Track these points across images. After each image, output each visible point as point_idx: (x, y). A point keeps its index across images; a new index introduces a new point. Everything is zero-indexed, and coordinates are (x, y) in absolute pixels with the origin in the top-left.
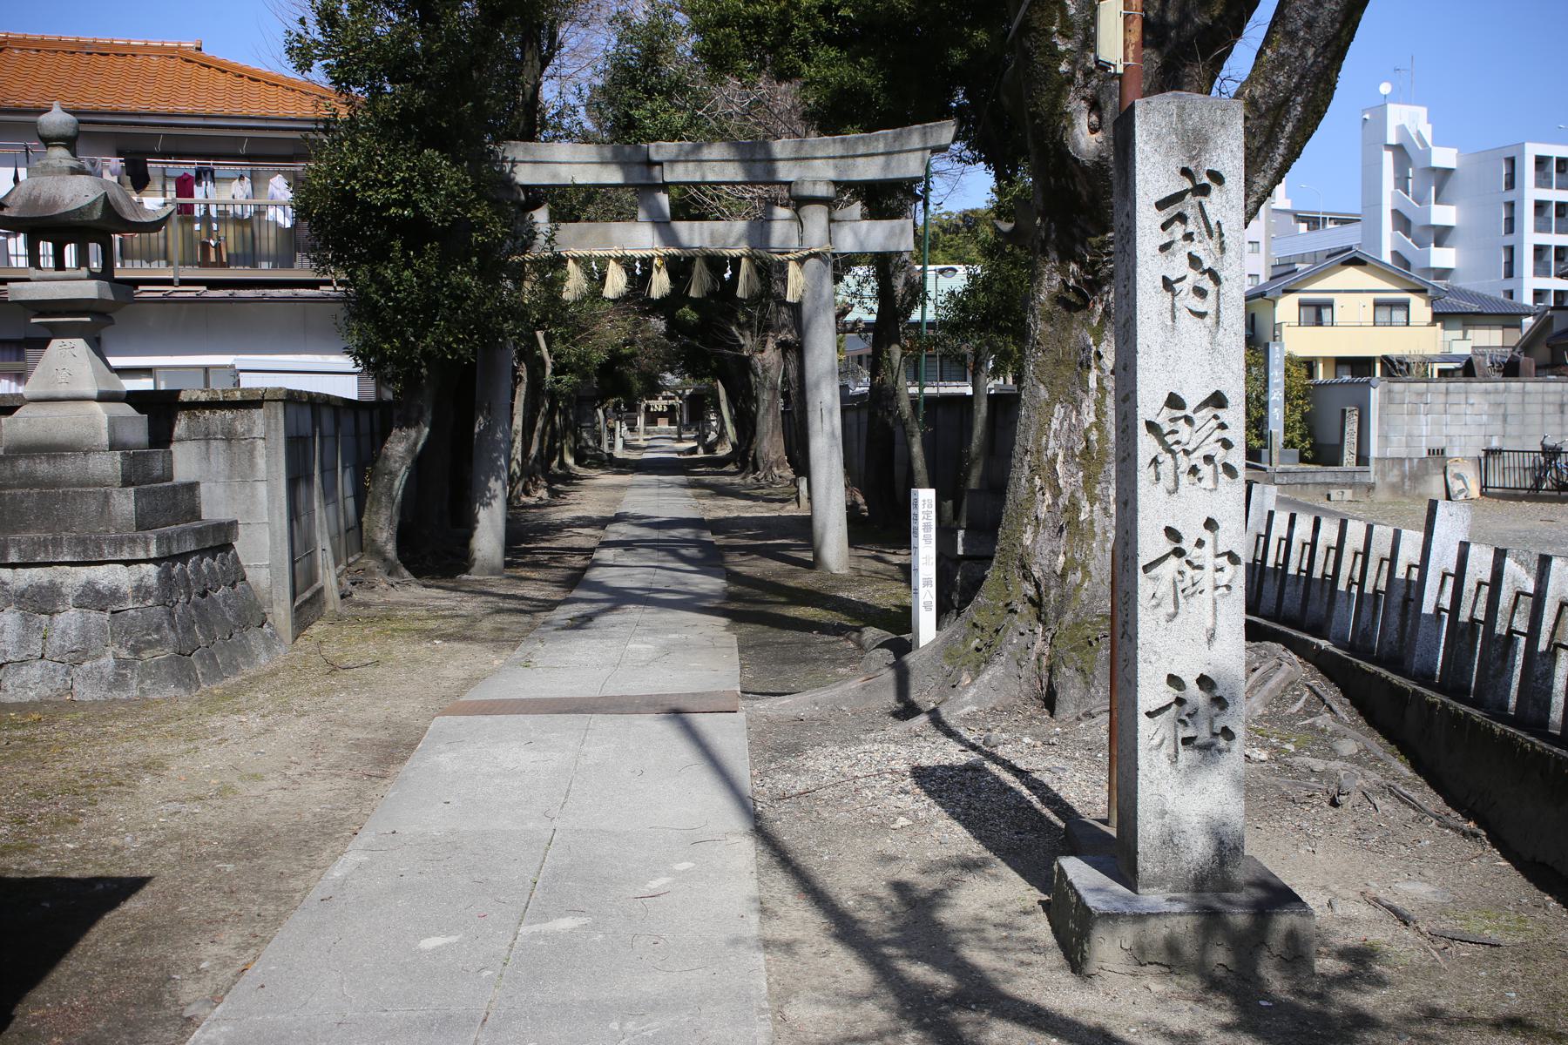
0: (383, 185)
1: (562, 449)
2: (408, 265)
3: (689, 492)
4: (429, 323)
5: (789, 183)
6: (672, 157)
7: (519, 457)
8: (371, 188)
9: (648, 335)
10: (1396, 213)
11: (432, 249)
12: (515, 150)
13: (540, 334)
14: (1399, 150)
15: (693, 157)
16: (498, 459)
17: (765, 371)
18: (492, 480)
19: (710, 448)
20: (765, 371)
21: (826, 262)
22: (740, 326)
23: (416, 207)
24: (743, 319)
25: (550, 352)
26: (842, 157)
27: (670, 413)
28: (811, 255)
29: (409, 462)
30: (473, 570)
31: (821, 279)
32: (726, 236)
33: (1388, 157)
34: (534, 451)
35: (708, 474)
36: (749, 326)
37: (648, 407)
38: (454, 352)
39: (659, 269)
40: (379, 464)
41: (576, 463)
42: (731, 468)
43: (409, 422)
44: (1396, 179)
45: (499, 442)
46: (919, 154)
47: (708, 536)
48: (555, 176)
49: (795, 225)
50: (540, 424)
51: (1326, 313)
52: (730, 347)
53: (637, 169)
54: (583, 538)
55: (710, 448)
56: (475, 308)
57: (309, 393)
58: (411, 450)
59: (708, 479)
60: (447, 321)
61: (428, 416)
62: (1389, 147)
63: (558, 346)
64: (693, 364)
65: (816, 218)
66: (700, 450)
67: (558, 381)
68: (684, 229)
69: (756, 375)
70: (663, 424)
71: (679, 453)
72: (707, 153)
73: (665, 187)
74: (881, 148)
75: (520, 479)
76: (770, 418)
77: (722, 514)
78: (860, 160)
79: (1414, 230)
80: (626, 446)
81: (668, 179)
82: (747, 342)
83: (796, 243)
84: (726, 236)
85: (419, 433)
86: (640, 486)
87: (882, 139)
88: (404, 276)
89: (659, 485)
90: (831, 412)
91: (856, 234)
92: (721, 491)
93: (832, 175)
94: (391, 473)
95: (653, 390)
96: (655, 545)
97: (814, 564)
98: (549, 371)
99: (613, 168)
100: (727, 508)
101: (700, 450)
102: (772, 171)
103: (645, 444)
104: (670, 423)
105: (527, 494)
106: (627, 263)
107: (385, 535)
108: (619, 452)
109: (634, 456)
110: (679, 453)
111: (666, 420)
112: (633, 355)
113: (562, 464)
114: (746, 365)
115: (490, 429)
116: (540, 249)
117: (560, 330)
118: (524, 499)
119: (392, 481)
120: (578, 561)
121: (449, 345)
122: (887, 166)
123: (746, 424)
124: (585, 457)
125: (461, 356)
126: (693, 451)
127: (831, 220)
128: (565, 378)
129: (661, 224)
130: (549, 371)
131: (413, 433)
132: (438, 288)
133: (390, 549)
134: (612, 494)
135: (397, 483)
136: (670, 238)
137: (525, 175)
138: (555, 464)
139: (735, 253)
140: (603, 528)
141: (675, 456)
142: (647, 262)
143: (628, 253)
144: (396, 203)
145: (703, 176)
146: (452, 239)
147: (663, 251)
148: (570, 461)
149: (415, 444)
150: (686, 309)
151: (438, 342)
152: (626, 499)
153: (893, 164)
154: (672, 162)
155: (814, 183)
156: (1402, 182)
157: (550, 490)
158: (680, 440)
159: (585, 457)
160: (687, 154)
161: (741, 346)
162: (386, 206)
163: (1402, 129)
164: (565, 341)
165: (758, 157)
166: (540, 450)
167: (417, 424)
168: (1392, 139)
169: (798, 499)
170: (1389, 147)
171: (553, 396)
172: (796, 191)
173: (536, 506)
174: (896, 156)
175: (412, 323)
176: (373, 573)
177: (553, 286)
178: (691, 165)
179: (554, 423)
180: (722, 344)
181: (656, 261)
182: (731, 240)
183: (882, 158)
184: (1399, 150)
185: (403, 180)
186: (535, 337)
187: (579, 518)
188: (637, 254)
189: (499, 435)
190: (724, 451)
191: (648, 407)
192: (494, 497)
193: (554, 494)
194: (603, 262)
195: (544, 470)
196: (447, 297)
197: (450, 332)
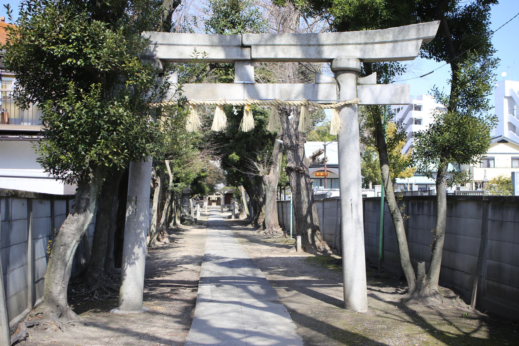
0: (63, 42)
1: (175, 217)
2: (79, 98)
3: (236, 239)
4: (94, 141)
5: (330, 61)
6: (256, 42)
7: (155, 223)
8: (54, 44)
9: (211, 168)
10: (510, 124)
11: (96, 87)
12: (157, 37)
13: (167, 162)
14: (510, 98)
15: (270, 43)
16: (140, 233)
17: (270, 183)
18: (136, 247)
19: (237, 216)
20: (270, 183)
21: (354, 109)
22: (258, 162)
23: (86, 59)
24: (259, 159)
25: (172, 171)
26: (366, 44)
27: (218, 202)
28: (346, 105)
29: (78, 237)
30: (121, 307)
31: (351, 120)
32: (289, 93)
33: (506, 101)
34: (162, 220)
35: (240, 229)
36: (262, 162)
37: (209, 198)
38: (110, 161)
39: (247, 112)
40: (57, 238)
41: (181, 223)
42: (250, 226)
43: (79, 209)
44: (509, 110)
45: (141, 223)
46: (414, 42)
47: (261, 274)
48: (181, 54)
49: (335, 86)
50: (166, 207)
51: (491, 162)
52: (254, 172)
53: (235, 50)
54: (186, 273)
55: (237, 216)
56: (127, 130)
57: (9, 190)
58: (79, 229)
59: (242, 232)
60: (106, 139)
61: (93, 206)
62: (506, 97)
63: (176, 169)
64: (231, 180)
65: (348, 81)
66: (233, 217)
67: (176, 186)
68: (262, 88)
69: (265, 185)
70: (214, 205)
71: (224, 218)
72: (278, 40)
73: (252, 61)
74: (391, 38)
75: (155, 234)
76: (272, 204)
77: (258, 255)
78: (377, 46)
79: (517, 130)
80: (202, 215)
81: (254, 56)
82: (261, 170)
83: (334, 97)
84: (289, 93)
85: (86, 217)
86: (212, 236)
87: (391, 33)
88: (76, 108)
89: (221, 235)
90: (357, 206)
91: (373, 93)
92: (252, 240)
93: (359, 55)
94: (65, 245)
95: (213, 191)
96: (233, 281)
97: (343, 305)
98: (171, 181)
99: (219, 49)
100: (258, 250)
101: (233, 217)
102: (319, 52)
103: (208, 213)
104: (217, 204)
105: (158, 240)
106: (227, 109)
107: (59, 288)
108: (199, 218)
109: (204, 219)
110: (224, 218)
111: (215, 203)
112: (206, 176)
113: (175, 224)
114: (259, 180)
115: (135, 214)
116: (172, 97)
117: (178, 161)
118: (157, 243)
119: (65, 250)
120: (187, 294)
121: (106, 157)
122: (394, 49)
123: (256, 207)
124: (184, 220)
125: (115, 165)
126: (230, 217)
127: (358, 84)
128: (179, 185)
129: (248, 85)
130: (171, 181)
131: (81, 217)
132: (100, 116)
133: (62, 299)
134: (199, 240)
135: (69, 252)
136: (254, 94)
137: (162, 53)
138: (171, 224)
139: (297, 103)
140: (200, 264)
141: (222, 219)
142: (241, 109)
143: (228, 103)
144: (71, 55)
145: (276, 54)
146: (111, 81)
147: (251, 102)
148: (178, 222)
149: (83, 225)
150: (234, 154)
151: (99, 155)
152: (207, 244)
153: (398, 48)
154: (257, 45)
155: (349, 59)
156: (512, 111)
157: (169, 238)
158: (222, 212)
159: (184, 220)
160: (267, 41)
161: (258, 172)
162: (64, 57)
163: (512, 90)
164: (179, 166)
165: (312, 43)
166: (166, 219)
167: (85, 211)
168: (508, 95)
169: (296, 247)
170: (506, 97)
171: (173, 192)
172: (335, 65)
173: (163, 248)
174: (400, 43)
175: (83, 142)
176: (47, 317)
177: (179, 121)
178: (268, 48)
179: (172, 206)
180: (250, 170)
181: (246, 108)
182: (293, 96)
183: (391, 45)
184: (510, 98)
185: (77, 39)
186: (165, 164)
187: (185, 257)
188: (234, 103)
189: (142, 218)
190: (243, 217)
191: (209, 198)
192: (137, 259)
193: (172, 240)
194: (213, 108)
195: (169, 229)
196: (106, 122)
197: (107, 147)
